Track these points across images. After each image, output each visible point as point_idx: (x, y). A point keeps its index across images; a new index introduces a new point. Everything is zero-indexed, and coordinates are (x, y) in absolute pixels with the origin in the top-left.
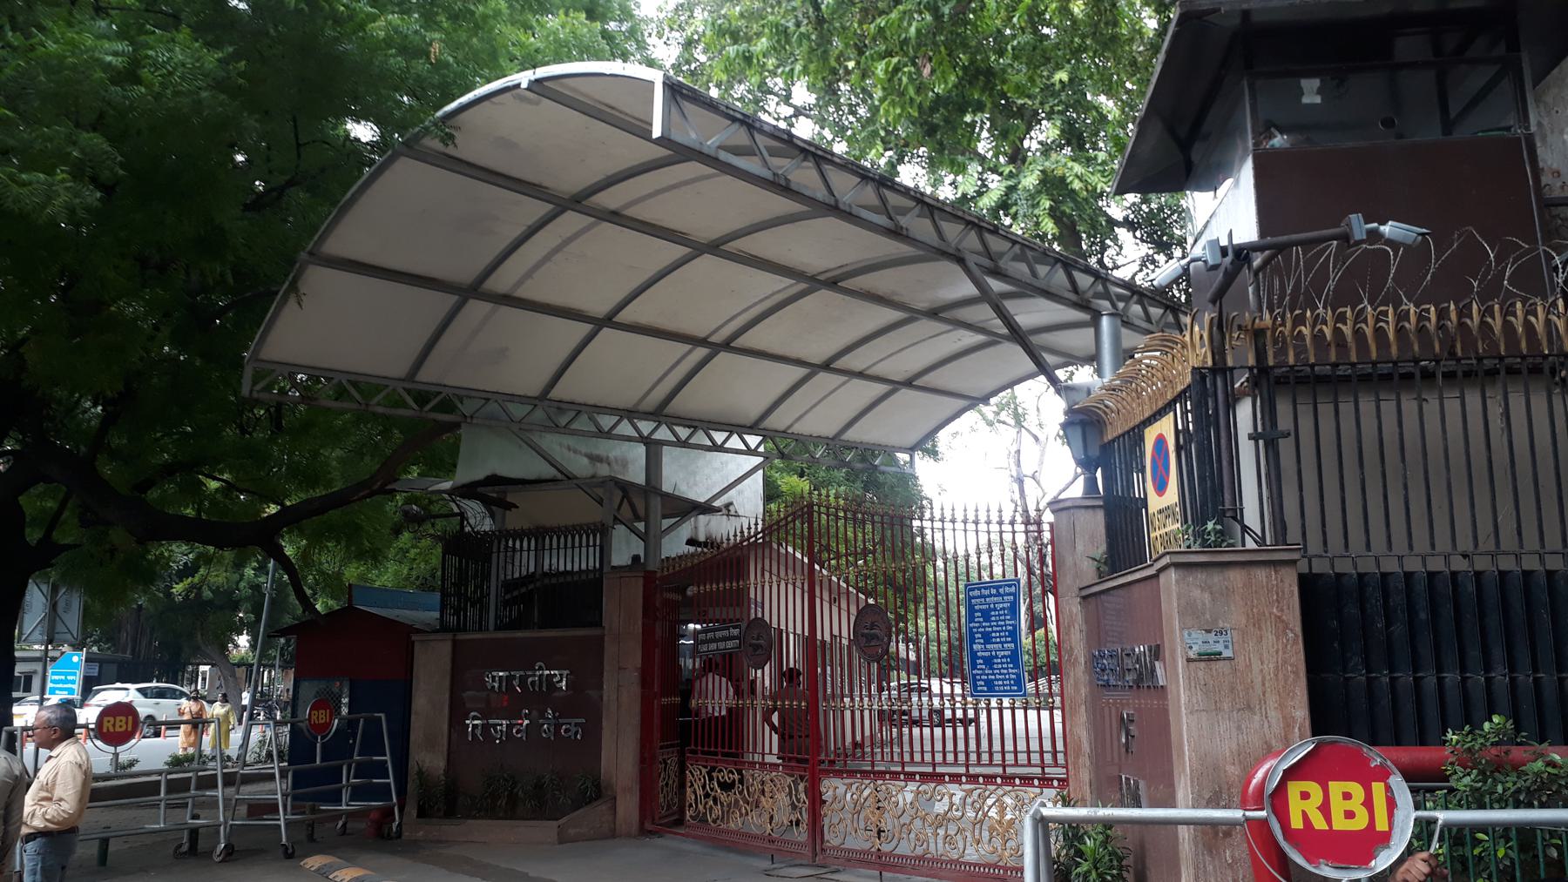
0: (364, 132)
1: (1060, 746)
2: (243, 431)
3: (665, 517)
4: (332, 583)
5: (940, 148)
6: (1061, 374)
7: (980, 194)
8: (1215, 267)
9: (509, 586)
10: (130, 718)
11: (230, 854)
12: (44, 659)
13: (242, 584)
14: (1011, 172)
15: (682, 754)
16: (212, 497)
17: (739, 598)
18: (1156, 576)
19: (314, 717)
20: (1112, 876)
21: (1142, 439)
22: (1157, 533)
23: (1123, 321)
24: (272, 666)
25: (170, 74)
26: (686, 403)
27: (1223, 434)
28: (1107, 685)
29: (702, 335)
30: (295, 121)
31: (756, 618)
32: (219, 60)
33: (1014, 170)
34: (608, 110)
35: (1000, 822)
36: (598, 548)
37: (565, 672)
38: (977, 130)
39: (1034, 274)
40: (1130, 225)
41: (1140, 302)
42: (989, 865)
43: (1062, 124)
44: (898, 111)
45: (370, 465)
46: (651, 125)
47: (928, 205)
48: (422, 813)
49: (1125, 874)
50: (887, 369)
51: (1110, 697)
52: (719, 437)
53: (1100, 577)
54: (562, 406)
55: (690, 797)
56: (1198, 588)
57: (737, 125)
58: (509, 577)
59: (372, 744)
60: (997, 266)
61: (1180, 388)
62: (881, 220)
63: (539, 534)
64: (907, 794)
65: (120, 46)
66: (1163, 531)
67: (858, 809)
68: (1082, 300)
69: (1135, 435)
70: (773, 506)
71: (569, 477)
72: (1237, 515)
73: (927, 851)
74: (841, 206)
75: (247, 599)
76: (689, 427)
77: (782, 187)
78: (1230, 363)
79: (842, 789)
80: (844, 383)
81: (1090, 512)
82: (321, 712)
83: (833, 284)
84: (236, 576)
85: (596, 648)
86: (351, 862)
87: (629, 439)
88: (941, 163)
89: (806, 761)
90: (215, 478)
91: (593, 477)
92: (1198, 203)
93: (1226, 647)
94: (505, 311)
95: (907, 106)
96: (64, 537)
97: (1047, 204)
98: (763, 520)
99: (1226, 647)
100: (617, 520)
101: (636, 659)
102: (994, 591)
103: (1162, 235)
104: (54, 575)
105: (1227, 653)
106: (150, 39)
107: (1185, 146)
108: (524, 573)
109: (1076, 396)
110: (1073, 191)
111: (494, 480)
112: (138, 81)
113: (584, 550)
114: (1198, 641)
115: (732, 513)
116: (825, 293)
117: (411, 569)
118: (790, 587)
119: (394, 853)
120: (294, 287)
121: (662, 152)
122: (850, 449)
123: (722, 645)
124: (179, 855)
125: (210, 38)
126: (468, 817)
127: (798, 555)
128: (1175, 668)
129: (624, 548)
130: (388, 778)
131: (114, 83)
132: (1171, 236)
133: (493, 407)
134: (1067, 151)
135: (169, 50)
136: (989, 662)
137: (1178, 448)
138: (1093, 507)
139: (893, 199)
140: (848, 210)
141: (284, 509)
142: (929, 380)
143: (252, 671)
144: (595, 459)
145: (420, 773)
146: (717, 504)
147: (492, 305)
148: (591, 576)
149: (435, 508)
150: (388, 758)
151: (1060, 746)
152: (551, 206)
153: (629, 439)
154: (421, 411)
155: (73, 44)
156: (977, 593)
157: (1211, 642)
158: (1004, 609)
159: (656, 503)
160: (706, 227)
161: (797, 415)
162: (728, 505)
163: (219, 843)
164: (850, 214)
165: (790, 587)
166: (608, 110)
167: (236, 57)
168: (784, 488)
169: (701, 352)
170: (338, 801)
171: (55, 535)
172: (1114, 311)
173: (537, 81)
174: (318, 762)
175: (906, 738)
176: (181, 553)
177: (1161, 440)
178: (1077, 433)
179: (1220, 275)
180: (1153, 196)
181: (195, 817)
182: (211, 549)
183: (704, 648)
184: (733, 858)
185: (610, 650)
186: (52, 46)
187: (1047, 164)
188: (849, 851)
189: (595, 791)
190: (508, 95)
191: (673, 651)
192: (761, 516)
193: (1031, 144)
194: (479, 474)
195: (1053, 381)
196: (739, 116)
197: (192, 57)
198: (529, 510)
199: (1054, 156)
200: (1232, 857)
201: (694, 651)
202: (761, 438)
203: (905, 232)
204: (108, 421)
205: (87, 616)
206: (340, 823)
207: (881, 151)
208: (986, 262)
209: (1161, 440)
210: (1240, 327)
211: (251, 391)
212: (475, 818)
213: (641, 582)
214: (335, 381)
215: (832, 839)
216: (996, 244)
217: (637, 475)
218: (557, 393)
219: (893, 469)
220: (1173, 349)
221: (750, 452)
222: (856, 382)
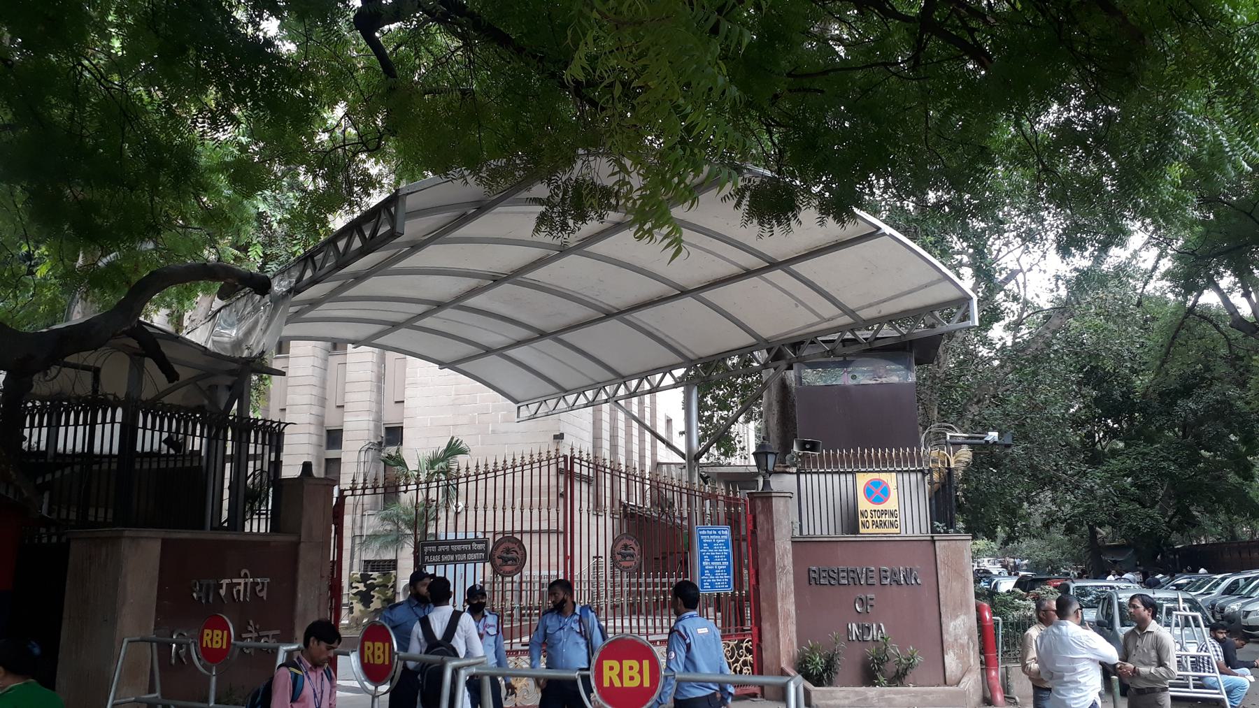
10: (646, 663)
82: (627, 663)
136: (712, 572)
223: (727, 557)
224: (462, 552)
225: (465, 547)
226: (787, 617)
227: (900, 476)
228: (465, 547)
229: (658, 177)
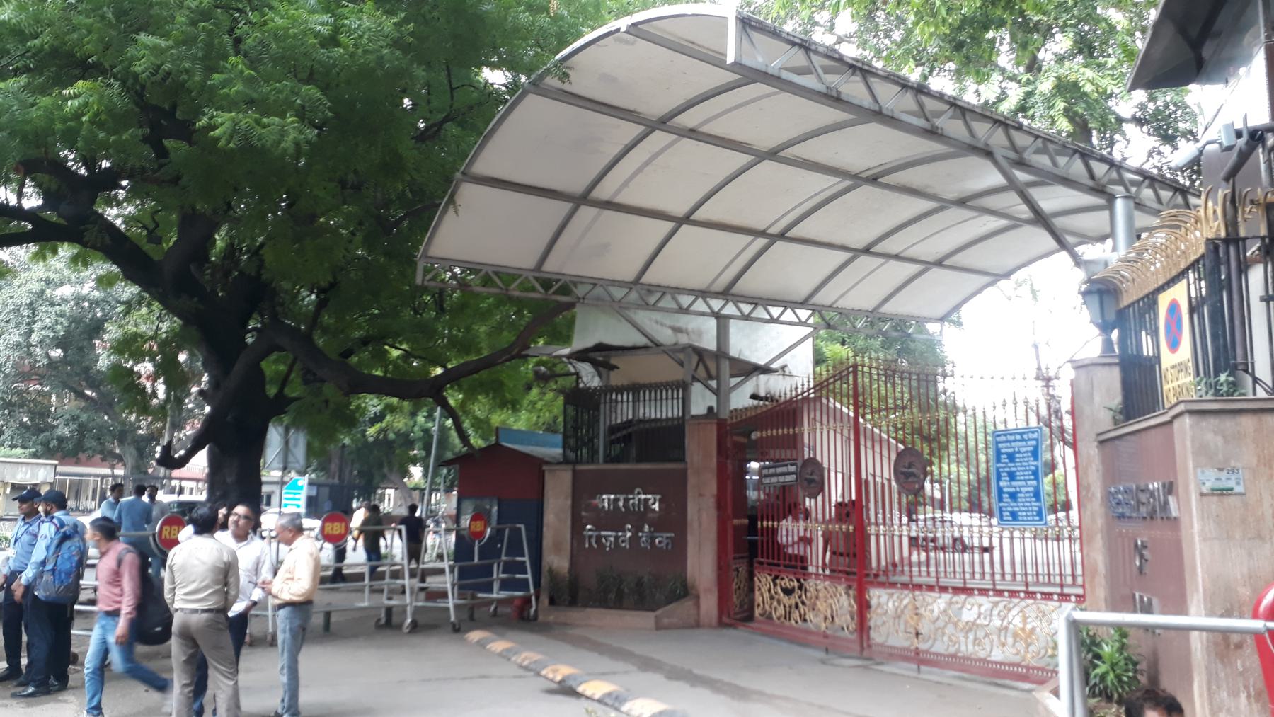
0: (496, 77)
1: (1079, 571)
2: (416, 312)
3: (732, 376)
4: (480, 424)
5: (968, 60)
6: (1080, 249)
7: (1000, 100)
8: (1229, 148)
9: (613, 429)
11: (415, 627)
12: (282, 483)
13: (416, 429)
14: (1028, 79)
15: (751, 565)
16: (394, 362)
17: (794, 442)
18: (1170, 422)
19: (472, 527)
20: (1128, 677)
21: (1155, 302)
22: (1170, 386)
23: (1136, 203)
24: (438, 490)
25: (361, 37)
26: (748, 284)
27: (1235, 296)
28: (1122, 516)
29: (762, 227)
30: (448, 70)
31: (810, 459)
32: (395, 24)
33: (1031, 78)
34: (689, 45)
35: (1023, 629)
36: (680, 401)
37: (658, 497)
38: (997, 45)
39: (1055, 164)
40: (1139, 121)
41: (1151, 186)
42: (1013, 665)
43: (1075, 36)
44: (932, 29)
45: (507, 337)
46: (726, 56)
47: (960, 107)
48: (552, 602)
49: (1139, 677)
50: (919, 251)
51: (1125, 527)
52: (775, 311)
53: (1115, 424)
54: (651, 289)
55: (758, 599)
56: (1210, 431)
57: (796, 48)
58: (613, 422)
59: (515, 549)
60: (1022, 158)
61: (1193, 258)
62: (920, 122)
63: (635, 389)
64: (939, 603)
65: (326, 18)
66: (1175, 384)
67: (898, 616)
68: (1098, 185)
69: (1150, 301)
70: (818, 369)
71: (658, 345)
72: (1248, 368)
73: (958, 650)
74: (885, 111)
75: (420, 439)
76: (751, 304)
77: (834, 99)
78: (1242, 233)
79: (884, 598)
80: (882, 264)
81: (1107, 368)
83: (873, 180)
84: (411, 423)
85: (682, 477)
86: (502, 636)
87: (703, 314)
88: (968, 74)
89: (854, 573)
90: (396, 348)
91: (675, 344)
92: (1198, 95)
93: (1238, 483)
94: (608, 214)
95: (940, 25)
96: (295, 390)
97: (1061, 105)
98: (814, 378)
99: (1238, 483)
100: (695, 379)
101: (712, 488)
102: (1018, 437)
103: (1168, 129)
104: (286, 419)
105: (1238, 489)
106: (345, 11)
107: (1196, 45)
108: (625, 419)
109: (1093, 268)
110: (1085, 94)
111: (601, 347)
112: (337, 44)
113: (670, 402)
114: (1211, 479)
115: (787, 373)
116: (867, 189)
117: (539, 417)
118: (832, 433)
119: (532, 631)
120: (452, 201)
121: (731, 77)
122: (885, 321)
123: (781, 479)
124: (379, 627)
125: (388, 6)
126: (586, 606)
127: (845, 410)
128: (1188, 501)
129: (701, 401)
130: (526, 573)
131: (323, 46)
132: (1176, 130)
133: (599, 291)
134: (1080, 59)
135: (360, 19)
136: (1013, 496)
137: (1192, 310)
138: (1110, 364)
139: (930, 104)
140: (890, 114)
141: (447, 371)
142: (959, 259)
143: (424, 495)
144: (677, 330)
145: (551, 571)
146: (774, 366)
147: (598, 210)
148: (676, 422)
149: (558, 369)
150: (526, 559)
151: (1079, 571)
152: (643, 128)
153: (703, 314)
154: (546, 294)
155: (294, 20)
156: (1003, 438)
157: (1223, 479)
158: (1027, 452)
159: (725, 366)
160: (765, 137)
161: (842, 292)
162: (783, 368)
163: (406, 619)
164: (892, 118)
165: (832, 433)
166: (689, 45)
167: (406, 21)
168: (828, 354)
169: (762, 242)
170: (491, 591)
171: (287, 391)
172: (1126, 194)
173: (634, 25)
174: (476, 560)
175: (932, 562)
176: (373, 404)
177: (1174, 306)
178: (1095, 300)
179: (1234, 156)
180: (1159, 94)
181: (390, 599)
182: (395, 400)
183: (767, 481)
184: (796, 648)
185: (692, 481)
186: (279, 21)
187: (1061, 71)
188: (891, 647)
189: (682, 591)
190: (610, 38)
191: (741, 485)
192: (811, 376)
193: (1046, 56)
194: (590, 343)
195: (1074, 256)
196: (797, 41)
197: (375, 23)
198: (627, 370)
199: (1067, 63)
200: (1243, 666)
201: (758, 486)
202: (810, 312)
203: (939, 131)
204: (321, 305)
205: (310, 451)
206: (492, 608)
207: (913, 66)
208: (1012, 155)
209: (1174, 306)
210: (1252, 202)
211: (423, 281)
212: (592, 607)
213: (714, 428)
214: (482, 273)
215: (876, 637)
216: (1021, 139)
217: (710, 343)
218: (648, 278)
219: (925, 337)
220: (1186, 223)
221: (802, 324)
222: (893, 263)
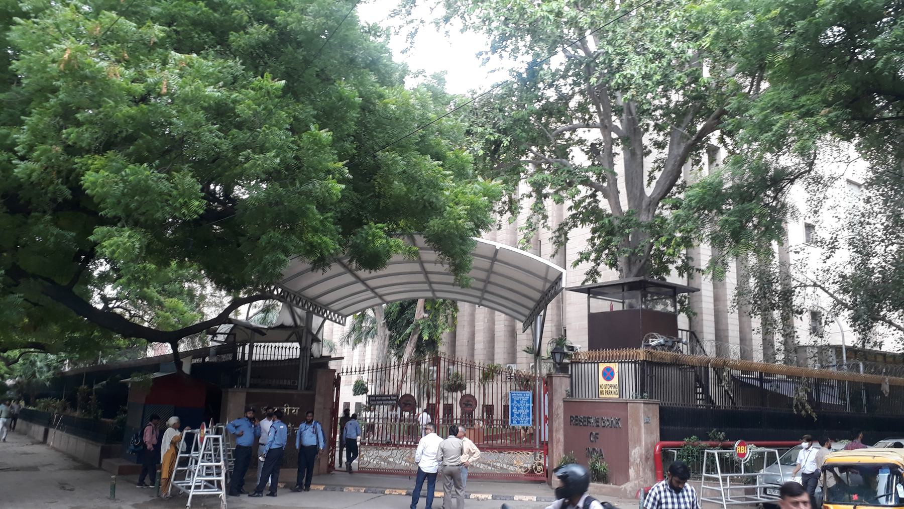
136: (519, 415)
223: (529, 408)
224: (386, 400)
225: (388, 398)
226: (558, 441)
227: (620, 365)
228: (388, 398)
229: (803, 152)
